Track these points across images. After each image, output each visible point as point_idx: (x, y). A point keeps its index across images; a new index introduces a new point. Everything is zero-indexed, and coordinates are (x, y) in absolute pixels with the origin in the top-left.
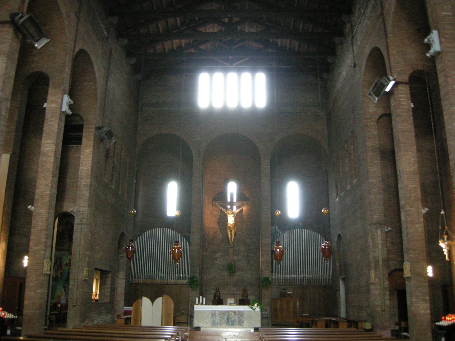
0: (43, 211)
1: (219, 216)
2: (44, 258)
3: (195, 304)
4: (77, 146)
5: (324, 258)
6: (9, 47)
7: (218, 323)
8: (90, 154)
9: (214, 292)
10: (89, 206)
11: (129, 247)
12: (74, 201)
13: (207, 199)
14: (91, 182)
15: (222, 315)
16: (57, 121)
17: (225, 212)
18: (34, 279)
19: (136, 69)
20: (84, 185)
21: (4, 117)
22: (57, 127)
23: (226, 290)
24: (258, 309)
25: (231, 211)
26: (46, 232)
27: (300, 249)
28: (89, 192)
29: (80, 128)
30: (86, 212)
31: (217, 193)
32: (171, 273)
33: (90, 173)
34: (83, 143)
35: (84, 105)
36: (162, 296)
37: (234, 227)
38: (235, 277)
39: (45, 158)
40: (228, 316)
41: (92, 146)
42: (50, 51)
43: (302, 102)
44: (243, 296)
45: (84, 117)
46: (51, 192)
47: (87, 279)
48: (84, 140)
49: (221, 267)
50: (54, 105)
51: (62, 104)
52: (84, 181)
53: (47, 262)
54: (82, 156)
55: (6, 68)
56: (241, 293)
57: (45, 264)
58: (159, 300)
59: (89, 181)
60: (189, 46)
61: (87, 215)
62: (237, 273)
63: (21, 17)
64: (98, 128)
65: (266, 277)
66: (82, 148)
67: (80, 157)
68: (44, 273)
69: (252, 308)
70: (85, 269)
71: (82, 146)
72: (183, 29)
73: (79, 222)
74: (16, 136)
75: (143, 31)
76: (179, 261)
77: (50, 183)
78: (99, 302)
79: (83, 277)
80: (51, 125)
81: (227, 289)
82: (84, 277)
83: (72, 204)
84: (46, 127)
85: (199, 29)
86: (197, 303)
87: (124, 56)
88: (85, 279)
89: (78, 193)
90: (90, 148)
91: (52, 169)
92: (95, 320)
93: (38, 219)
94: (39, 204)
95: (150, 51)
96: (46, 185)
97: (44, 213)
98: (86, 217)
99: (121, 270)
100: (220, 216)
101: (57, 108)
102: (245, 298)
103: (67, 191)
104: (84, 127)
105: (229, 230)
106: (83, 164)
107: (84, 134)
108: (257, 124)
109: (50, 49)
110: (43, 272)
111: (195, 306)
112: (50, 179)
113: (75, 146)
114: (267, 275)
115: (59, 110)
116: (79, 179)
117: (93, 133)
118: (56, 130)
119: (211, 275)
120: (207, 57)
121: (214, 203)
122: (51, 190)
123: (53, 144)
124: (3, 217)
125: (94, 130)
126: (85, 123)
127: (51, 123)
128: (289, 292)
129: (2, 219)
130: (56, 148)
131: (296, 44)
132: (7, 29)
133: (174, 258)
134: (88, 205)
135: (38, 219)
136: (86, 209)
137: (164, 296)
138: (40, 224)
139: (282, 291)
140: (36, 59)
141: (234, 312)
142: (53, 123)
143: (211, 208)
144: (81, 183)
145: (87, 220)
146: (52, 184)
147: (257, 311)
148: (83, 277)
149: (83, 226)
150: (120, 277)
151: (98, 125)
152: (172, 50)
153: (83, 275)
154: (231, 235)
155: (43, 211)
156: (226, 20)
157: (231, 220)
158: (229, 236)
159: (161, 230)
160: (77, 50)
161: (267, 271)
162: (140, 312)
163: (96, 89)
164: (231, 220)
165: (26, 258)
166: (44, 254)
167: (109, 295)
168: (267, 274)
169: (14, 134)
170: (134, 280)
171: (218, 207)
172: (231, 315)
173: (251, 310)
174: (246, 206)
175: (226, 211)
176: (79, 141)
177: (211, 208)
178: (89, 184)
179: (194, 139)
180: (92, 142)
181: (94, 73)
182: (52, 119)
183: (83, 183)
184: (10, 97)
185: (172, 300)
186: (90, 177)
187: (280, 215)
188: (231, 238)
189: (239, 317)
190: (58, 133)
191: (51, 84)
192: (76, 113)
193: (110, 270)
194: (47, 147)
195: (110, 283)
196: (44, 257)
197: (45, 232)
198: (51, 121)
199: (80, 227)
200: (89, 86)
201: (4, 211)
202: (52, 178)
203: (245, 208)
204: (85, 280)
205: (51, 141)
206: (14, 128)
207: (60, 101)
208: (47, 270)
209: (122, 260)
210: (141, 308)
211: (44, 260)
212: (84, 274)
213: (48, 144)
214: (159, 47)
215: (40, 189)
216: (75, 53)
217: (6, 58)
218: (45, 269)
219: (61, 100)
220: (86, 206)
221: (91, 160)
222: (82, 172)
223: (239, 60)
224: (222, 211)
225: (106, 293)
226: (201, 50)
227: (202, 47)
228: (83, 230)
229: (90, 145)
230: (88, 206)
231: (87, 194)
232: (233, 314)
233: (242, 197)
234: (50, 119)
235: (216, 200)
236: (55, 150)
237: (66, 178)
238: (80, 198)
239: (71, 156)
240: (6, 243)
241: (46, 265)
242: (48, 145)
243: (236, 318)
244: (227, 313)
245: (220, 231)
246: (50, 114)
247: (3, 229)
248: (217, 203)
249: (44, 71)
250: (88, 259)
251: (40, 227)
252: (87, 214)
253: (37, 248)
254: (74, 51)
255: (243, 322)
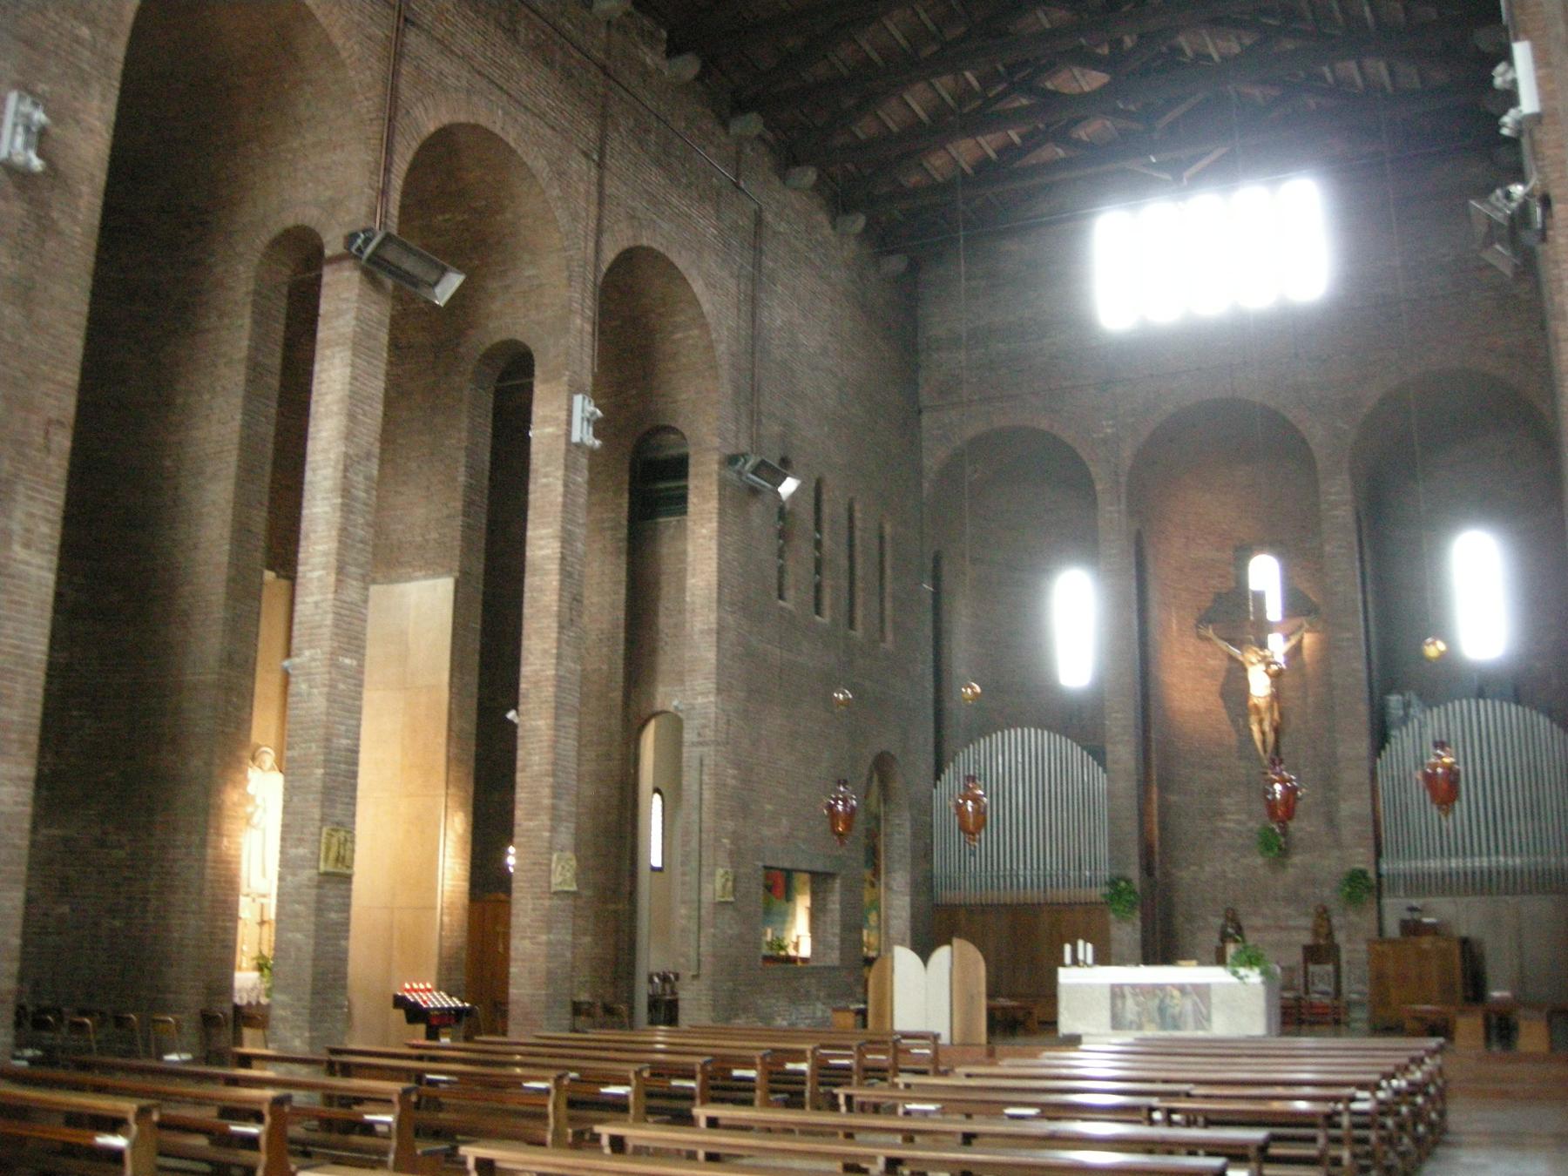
0: (541, 723)
1: (1223, 674)
2: (551, 849)
3: (1064, 965)
4: (678, 521)
5: (962, 834)
6: (354, 322)
7: (1131, 1023)
8: (711, 538)
9: (1219, 921)
10: (719, 691)
11: (836, 800)
12: (680, 678)
13: (1174, 621)
14: (720, 620)
15: (1142, 998)
16: (560, 473)
17: (1241, 658)
18: (530, 907)
19: (881, 239)
20: (702, 632)
21: (366, 504)
22: (560, 489)
23: (1264, 916)
24: (1254, 977)
25: (1256, 653)
26: (551, 780)
27: (1507, 769)
28: (715, 649)
29: (679, 467)
30: (713, 709)
31: (1211, 596)
32: (1035, 866)
33: (715, 595)
34: (691, 508)
35: (684, 396)
36: (949, 943)
37: (1270, 707)
38: (1291, 870)
39: (537, 578)
40: (1162, 1001)
41: (715, 517)
42: (529, 277)
43: (1447, 259)
44: (1316, 933)
45: (687, 434)
46: (557, 670)
47: (731, 899)
48: (693, 499)
49: (1240, 841)
50: (550, 430)
51: (569, 423)
52: (700, 618)
53: (559, 859)
54: (690, 548)
55: (354, 378)
56: (1307, 922)
57: (553, 865)
58: (942, 955)
59: (713, 617)
60: (1032, 141)
61: (717, 718)
62: (1296, 859)
63: (367, 241)
64: (732, 460)
65: (1354, 870)
66: (689, 524)
67: (685, 552)
68: (553, 890)
69: (1235, 973)
70: (720, 871)
71: (688, 518)
72: (994, 92)
73: (696, 739)
74: (467, 527)
75: (864, 129)
76: (977, 836)
77: (555, 645)
78: (813, 964)
79: (714, 894)
80: (546, 486)
81: (1266, 911)
82: (717, 894)
83: (676, 688)
84: (535, 492)
85: (1049, 85)
86: (1068, 959)
87: (822, 217)
88: (722, 900)
89: (687, 655)
90: (710, 520)
91: (555, 608)
92: (780, 1015)
93: (531, 746)
94: (530, 706)
95: (913, 179)
96: (545, 652)
97: (544, 728)
98: (712, 724)
99: (897, 866)
100: (1229, 671)
101: (558, 436)
102: (1322, 942)
103: (661, 652)
104: (691, 461)
105: (1253, 719)
106: (694, 569)
107: (692, 483)
108: (1296, 355)
109: (527, 274)
110: (549, 887)
111: (1061, 971)
112: (554, 635)
113: (672, 519)
114: (1362, 862)
115: (562, 441)
116: (688, 615)
117: (715, 477)
118: (560, 499)
119: (1207, 869)
120: (1089, 171)
121: (1203, 632)
122: (558, 664)
123: (553, 537)
124: (448, 744)
125: (716, 467)
126: (691, 451)
127: (544, 480)
128: (1428, 917)
129: (448, 751)
130: (563, 547)
131: (1379, 68)
132: (347, 274)
133: (963, 827)
134: (718, 689)
135: (531, 746)
136: (712, 698)
137: (956, 941)
138: (537, 758)
139: (1407, 916)
140: (496, 306)
141: (1182, 989)
142: (551, 479)
143: (1191, 649)
144: (692, 627)
145: (717, 731)
146: (558, 648)
147: (1254, 984)
148: (714, 894)
149: (706, 749)
150: (895, 888)
151: (729, 451)
152: (983, 165)
153: (714, 890)
154: (1263, 733)
155: (541, 723)
156: (1104, 50)
157: (1259, 686)
158: (1257, 736)
159: (1015, 734)
160: (610, 255)
161: (1361, 850)
162: (889, 995)
163: (710, 347)
164: (1259, 686)
165: (511, 849)
166: (551, 837)
167: (837, 943)
168: (1360, 858)
169: (459, 521)
170: (947, 896)
171: (1216, 644)
172: (1172, 997)
173: (1234, 980)
174: (1307, 631)
175: (1243, 655)
176: (679, 502)
177: (1191, 649)
178: (714, 626)
179: (1095, 436)
180: (713, 505)
181: (695, 302)
182: (548, 469)
183: (698, 626)
184: (376, 450)
185: (980, 957)
186: (714, 605)
187: (1442, 655)
188: (1264, 742)
189: (1195, 1004)
190: (565, 505)
191: (538, 371)
192: (666, 423)
193: (831, 870)
194: (541, 548)
195: (838, 906)
196: (551, 848)
197: (547, 778)
198: (546, 476)
199: (698, 751)
200: (690, 342)
201: (450, 729)
202: (559, 633)
203: (1308, 640)
204: (721, 903)
205: (550, 530)
206: (459, 505)
207: (563, 415)
208: (564, 882)
209: (897, 836)
210: (892, 981)
211: (551, 854)
212: (718, 885)
213: (542, 538)
214: (937, 163)
215: (531, 664)
216: (604, 268)
217: (349, 353)
218: (556, 879)
219: (565, 413)
220: (710, 692)
221: (715, 556)
222: (693, 595)
223: (1195, 159)
224: (1232, 658)
225: (830, 938)
226: (1078, 143)
227: (1082, 133)
228: (706, 762)
229: (711, 513)
230: (714, 691)
231: (711, 655)
232: (1176, 993)
233: (1297, 605)
234: (543, 470)
235: (1210, 622)
236: (562, 553)
237: (656, 614)
238: (694, 671)
239: (664, 551)
240: (466, 816)
241: (560, 868)
242: (542, 543)
243: (1188, 1005)
244: (1158, 992)
245: (1232, 721)
246: (541, 456)
247: (451, 778)
248: (1211, 631)
249: (519, 338)
250: (732, 843)
251: (536, 768)
252: (713, 715)
253: (531, 824)
254: (597, 267)
255: (1208, 1019)
